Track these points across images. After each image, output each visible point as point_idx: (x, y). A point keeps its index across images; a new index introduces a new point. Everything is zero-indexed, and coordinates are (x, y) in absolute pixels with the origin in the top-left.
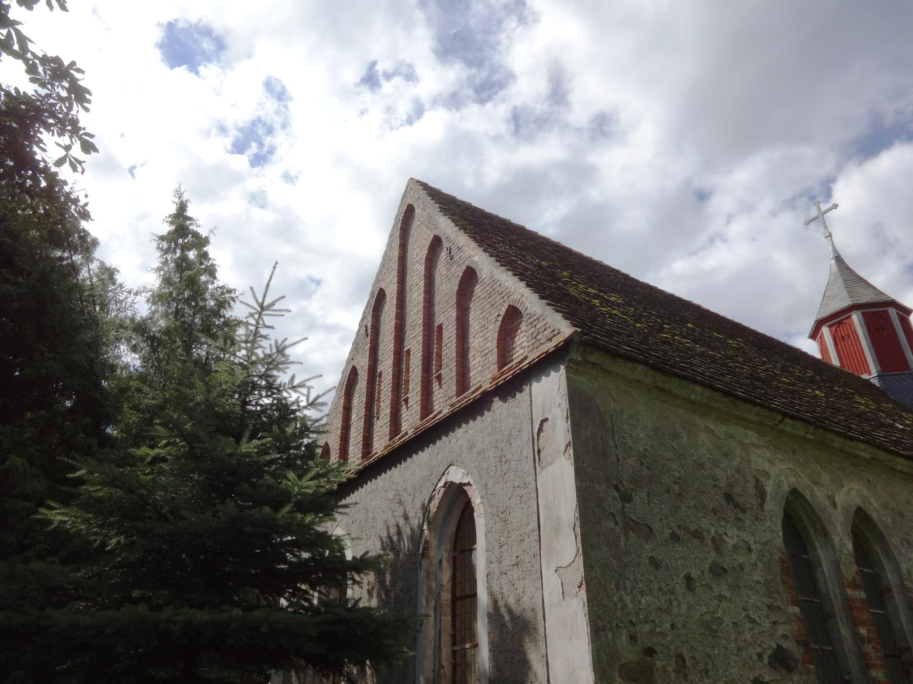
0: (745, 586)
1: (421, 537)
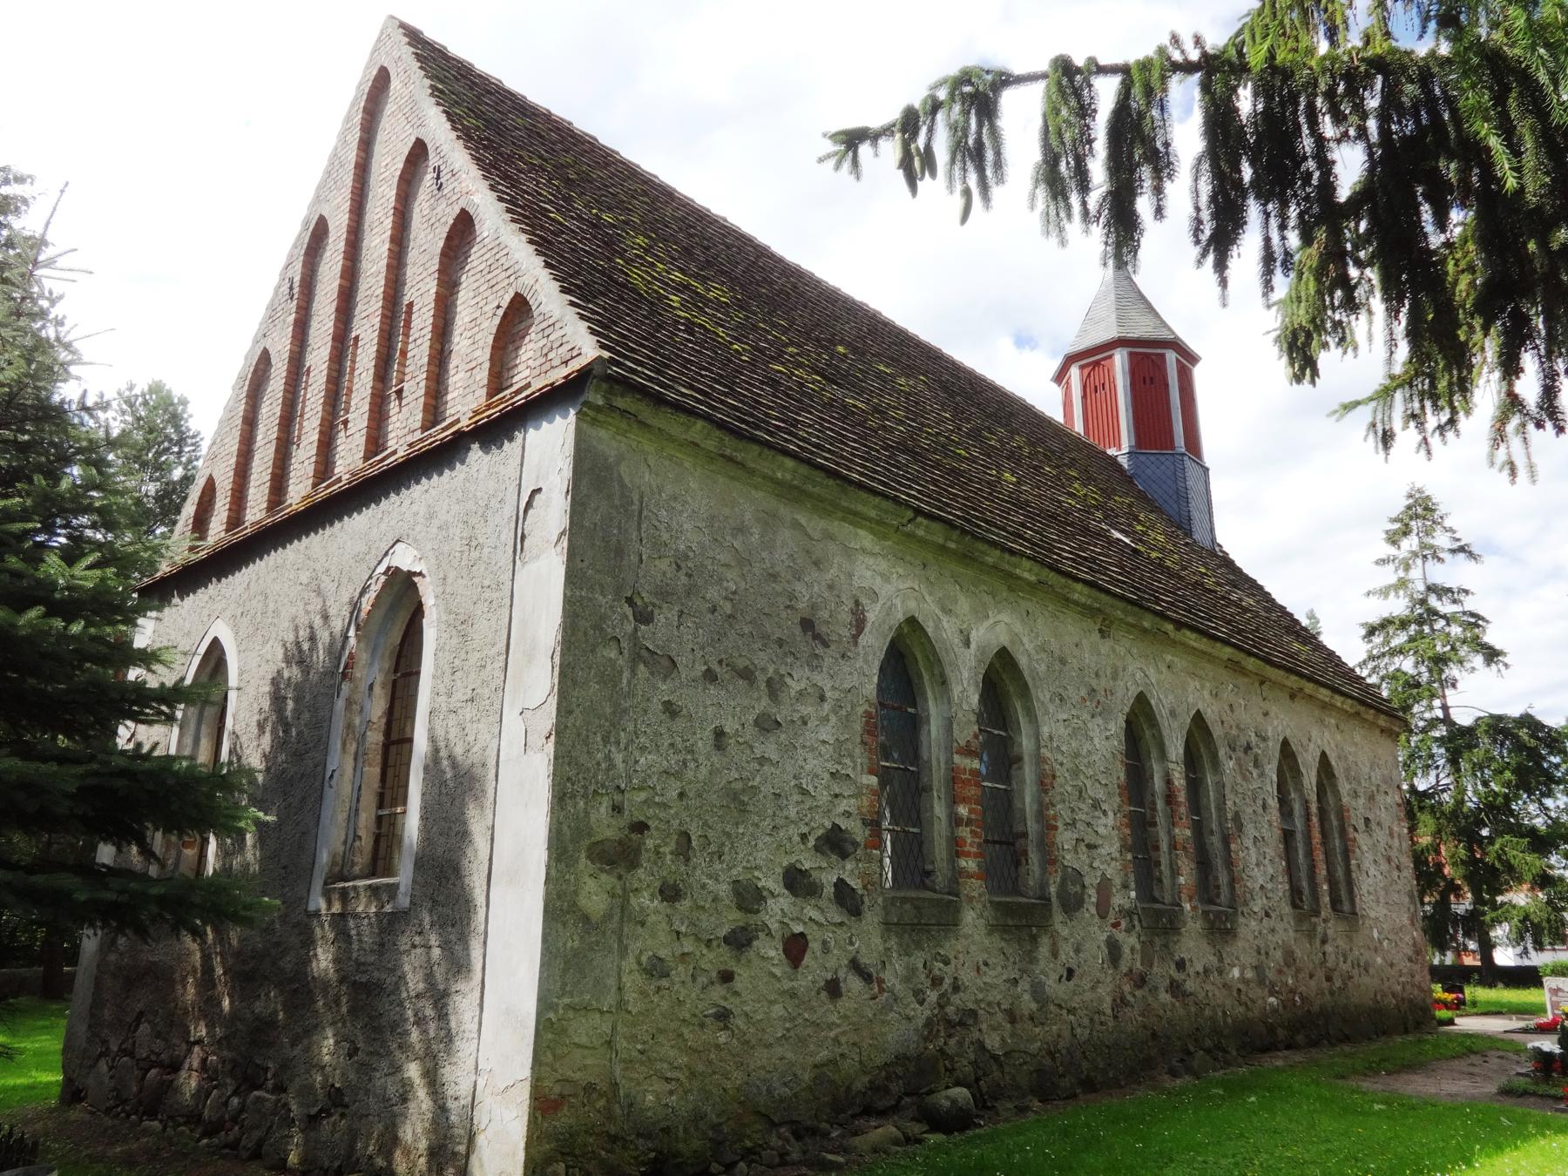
0: (804, 747)
1: (343, 647)
